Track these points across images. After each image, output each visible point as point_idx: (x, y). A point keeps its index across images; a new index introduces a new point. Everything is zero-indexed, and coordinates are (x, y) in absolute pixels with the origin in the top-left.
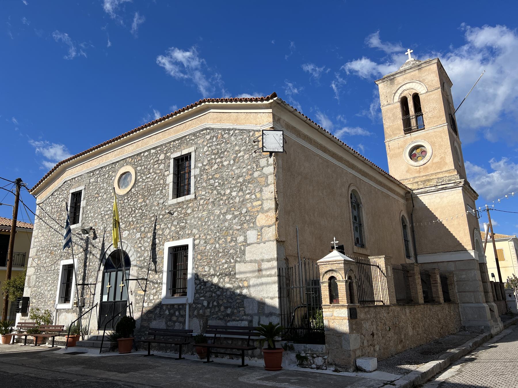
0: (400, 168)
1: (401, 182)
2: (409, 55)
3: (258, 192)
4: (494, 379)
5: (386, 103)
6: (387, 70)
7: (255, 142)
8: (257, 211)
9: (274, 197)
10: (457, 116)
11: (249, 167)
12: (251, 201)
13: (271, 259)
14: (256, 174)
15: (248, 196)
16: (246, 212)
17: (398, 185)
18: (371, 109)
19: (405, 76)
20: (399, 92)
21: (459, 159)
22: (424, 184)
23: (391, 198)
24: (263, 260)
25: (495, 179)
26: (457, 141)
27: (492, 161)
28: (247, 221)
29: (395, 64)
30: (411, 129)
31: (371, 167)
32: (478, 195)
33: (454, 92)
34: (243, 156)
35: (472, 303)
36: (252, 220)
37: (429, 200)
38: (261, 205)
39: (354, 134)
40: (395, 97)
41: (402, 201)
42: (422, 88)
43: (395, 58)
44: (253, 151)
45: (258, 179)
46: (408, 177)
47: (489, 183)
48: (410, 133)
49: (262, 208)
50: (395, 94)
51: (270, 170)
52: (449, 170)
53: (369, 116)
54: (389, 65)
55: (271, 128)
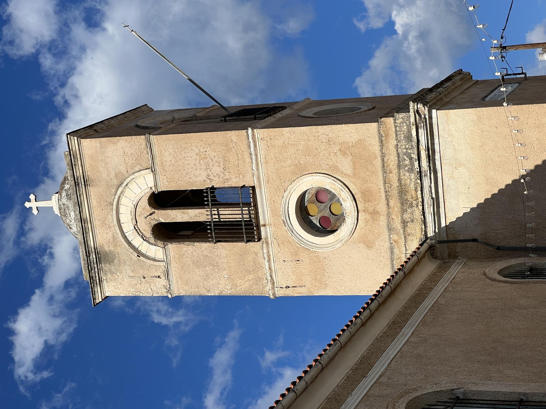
0: (356, 265)
1: (397, 266)
2: (41, 204)
5: (163, 281)
6: (64, 263)
10: (235, 101)
17: (406, 275)
18: (164, 321)
19: (96, 223)
20: (137, 241)
21: (352, 110)
22: (411, 206)
23: (442, 301)
25: (414, 20)
26: (301, 110)
27: (361, 26)
29: (51, 240)
30: (249, 224)
31: (341, 345)
32: (460, 72)
33: (164, 103)
37: (461, 196)
39: (229, 376)
40: (151, 254)
41: (456, 270)
42: (140, 181)
43: (34, 238)
46: (387, 245)
47: (423, 35)
48: (258, 227)
50: (140, 254)
52: (380, 136)
53: (186, 329)
54: (52, 255)
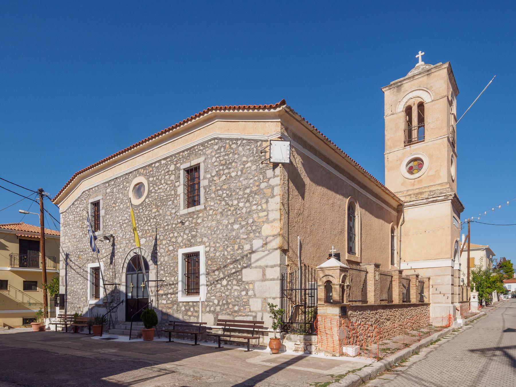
5: (390, 113)
7: (261, 153)
11: (256, 178)
12: (258, 212)
14: (263, 185)
15: (254, 207)
16: (253, 222)
19: (412, 82)
22: (416, 197)
24: (267, 266)
28: (254, 231)
34: (250, 167)
36: (258, 231)
44: (260, 162)
45: (264, 190)
48: (410, 145)
49: (268, 219)
51: (276, 181)
52: (442, 184)
55: (279, 138)
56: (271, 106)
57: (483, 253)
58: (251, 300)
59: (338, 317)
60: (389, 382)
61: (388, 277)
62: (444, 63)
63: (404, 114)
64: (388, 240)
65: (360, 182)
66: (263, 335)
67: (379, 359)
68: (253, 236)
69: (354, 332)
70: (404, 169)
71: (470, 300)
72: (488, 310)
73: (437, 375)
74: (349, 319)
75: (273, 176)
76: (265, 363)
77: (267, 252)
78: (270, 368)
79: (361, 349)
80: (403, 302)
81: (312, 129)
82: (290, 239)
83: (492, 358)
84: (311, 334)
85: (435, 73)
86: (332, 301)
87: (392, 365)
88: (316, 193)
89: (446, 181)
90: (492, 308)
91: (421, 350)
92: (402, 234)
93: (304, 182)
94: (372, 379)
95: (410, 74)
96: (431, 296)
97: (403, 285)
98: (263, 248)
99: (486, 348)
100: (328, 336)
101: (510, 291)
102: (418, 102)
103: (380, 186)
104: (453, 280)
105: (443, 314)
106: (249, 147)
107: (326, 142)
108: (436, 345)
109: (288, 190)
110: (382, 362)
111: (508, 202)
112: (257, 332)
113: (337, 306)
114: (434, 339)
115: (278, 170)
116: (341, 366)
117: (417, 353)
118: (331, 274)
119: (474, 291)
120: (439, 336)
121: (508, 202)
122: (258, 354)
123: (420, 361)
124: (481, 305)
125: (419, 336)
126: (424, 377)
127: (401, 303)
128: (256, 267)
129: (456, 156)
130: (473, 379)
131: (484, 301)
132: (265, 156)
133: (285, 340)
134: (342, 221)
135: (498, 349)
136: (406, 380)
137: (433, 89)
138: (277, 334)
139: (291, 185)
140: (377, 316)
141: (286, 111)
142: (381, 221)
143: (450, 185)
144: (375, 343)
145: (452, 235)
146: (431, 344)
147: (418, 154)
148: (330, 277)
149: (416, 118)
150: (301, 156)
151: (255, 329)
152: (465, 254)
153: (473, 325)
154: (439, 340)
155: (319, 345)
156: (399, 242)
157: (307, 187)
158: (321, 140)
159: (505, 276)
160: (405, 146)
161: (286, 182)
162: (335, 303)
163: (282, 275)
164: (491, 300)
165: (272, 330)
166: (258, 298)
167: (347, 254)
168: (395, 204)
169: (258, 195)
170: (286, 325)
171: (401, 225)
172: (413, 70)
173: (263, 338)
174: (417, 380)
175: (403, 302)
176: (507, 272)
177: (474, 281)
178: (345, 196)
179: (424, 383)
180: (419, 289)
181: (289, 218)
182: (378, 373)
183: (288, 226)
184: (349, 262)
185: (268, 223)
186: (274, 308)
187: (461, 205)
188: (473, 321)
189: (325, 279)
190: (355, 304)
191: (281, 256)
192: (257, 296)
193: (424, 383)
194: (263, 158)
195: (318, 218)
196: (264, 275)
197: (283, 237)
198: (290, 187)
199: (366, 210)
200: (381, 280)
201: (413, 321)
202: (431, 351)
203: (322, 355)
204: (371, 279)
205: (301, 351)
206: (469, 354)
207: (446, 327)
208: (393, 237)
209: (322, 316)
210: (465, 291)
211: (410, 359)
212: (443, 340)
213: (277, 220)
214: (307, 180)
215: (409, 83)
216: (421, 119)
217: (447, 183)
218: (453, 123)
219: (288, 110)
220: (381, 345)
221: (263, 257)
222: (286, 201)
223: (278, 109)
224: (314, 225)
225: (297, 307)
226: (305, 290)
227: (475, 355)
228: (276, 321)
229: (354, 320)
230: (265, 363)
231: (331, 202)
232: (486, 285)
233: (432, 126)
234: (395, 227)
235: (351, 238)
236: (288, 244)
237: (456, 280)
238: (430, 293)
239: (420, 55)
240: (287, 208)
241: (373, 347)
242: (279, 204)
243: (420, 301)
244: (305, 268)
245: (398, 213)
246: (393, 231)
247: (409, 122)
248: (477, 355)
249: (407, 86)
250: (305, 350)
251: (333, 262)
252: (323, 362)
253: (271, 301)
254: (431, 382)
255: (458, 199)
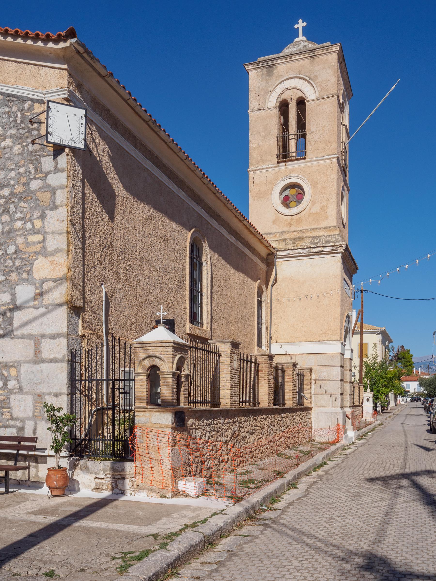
3: (38, 218)
4: (347, 502)
5: (257, 107)
7: (32, 123)
8: (36, 252)
9: (65, 229)
11: (22, 170)
12: (25, 233)
13: (58, 334)
14: (35, 185)
15: (19, 224)
16: (16, 252)
17: (260, 240)
19: (289, 65)
20: (279, 90)
22: (293, 243)
24: (43, 336)
28: (18, 268)
34: (11, 148)
35: (329, 407)
36: (25, 268)
38: (43, 241)
44: (29, 141)
45: (38, 194)
46: (274, 231)
48: (285, 161)
49: (44, 248)
51: (59, 179)
52: (329, 227)
55: (65, 99)
56: (48, 36)
57: (377, 339)
58: (12, 397)
59: (170, 430)
60: (252, 541)
61: (252, 365)
62: (333, 43)
63: (276, 112)
64: (253, 307)
65: (210, 208)
66: (37, 462)
67: (237, 500)
68: (16, 279)
69: (197, 454)
70: (276, 198)
71: (362, 403)
72: (385, 417)
73: (325, 524)
74: (189, 433)
75: (53, 169)
76: (33, 518)
77: (42, 310)
78: (41, 527)
79: (207, 483)
80: (275, 404)
81: (127, 97)
82: (87, 289)
83: (397, 491)
84: (124, 459)
85: (322, 57)
86: (159, 401)
87: (257, 508)
88: (137, 217)
89: (335, 224)
90: (389, 415)
91: (299, 481)
92: (273, 299)
93: (113, 191)
94: (224, 537)
95: (286, 51)
96: (313, 396)
97: (274, 379)
98: (36, 302)
99: (387, 475)
100: (153, 462)
101: (409, 392)
102: (297, 97)
103: (242, 219)
104: (342, 374)
105: (330, 424)
106: (7, 109)
107: (153, 125)
108: (320, 472)
109: (83, 198)
110: (242, 506)
111: (417, 261)
112: (26, 458)
113: (168, 411)
114: (318, 463)
115: (63, 160)
116: (174, 515)
117: (294, 486)
118: (157, 354)
119: (368, 390)
120: (324, 458)
121: (417, 261)
122: (24, 498)
123: (299, 499)
124: (376, 410)
125: (297, 457)
126: (306, 529)
127: (272, 406)
128: (23, 337)
129: (348, 190)
130: (376, 529)
131: (380, 406)
132: (38, 129)
133: (77, 471)
134: (181, 267)
135: (404, 476)
136: (278, 535)
137: (318, 80)
138: (61, 460)
139: (89, 190)
140: (235, 428)
141: (78, 52)
142: (242, 275)
143: (340, 231)
144: (232, 471)
145: (342, 306)
146: (314, 471)
147: (297, 178)
148: (156, 359)
149: (294, 116)
150: (107, 143)
151: (21, 452)
152: (357, 338)
153: (367, 440)
154: (325, 463)
155: (138, 478)
156: (269, 312)
157: (119, 200)
158: (144, 120)
159: (404, 371)
160: (278, 163)
161: (79, 184)
162: (164, 406)
163: (72, 353)
164: (388, 403)
165: (52, 453)
166: (26, 393)
167: (188, 324)
168: (263, 252)
169: (26, 202)
170: (80, 444)
171: (272, 286)
172: (290, 46)
173: (37, 467)
174: (295, 535)
175: (275, 404)
176: (406, 366)
177: (367, 377)
178: (187, 226)
179: (305, 539)
180: (297, 385)
181: (84, 251)
182: (236, 524)
183: (84, 265)
184: (192, 337)
185: (45, 256)
186: (56, 413)
187: (355, 263)
188: (367, 433)
189: (148, 363)
190: (200, 407)
191: (70, 318)
192: (25, 390)
193: (305, 539)
194: (35, 133)
195: (139, 257)
196: (38, 351)
197: (74, 284)
198: (87, 195)
199: (220, 255)
200: (242, 369)
201: (288, 435)
202: (315, 482)
203: (142, 497)
204: (226, 366)
205: (106, 490)
206: (367, 485)
207: (334, 443)
208: (260, 303)
209: (142, 428)
210: (356, 390)
211: (284, 496)
212: (330, 464)
213: (61, 251)
214: (119, 188)
215: (285, 65)
216: (301, 125)
217: (336, 227)
218: (344, 139)
219: (81, 50)
220: (241, 474)
221: (35, 319)
222: (78, 218)
223: (62, 45)
224: (132, 268)
225: (101, 411)
226: (114, 381)
227: (376, 487)
228: (59, 437)
229: (197, 434)
230: (33, 518)
231: (161, 232)
232: (382, 381)
233: (316, 137)
234: (264, 287)
235: (195, 298)
236: (84, 298)
237: (347, 373)
238: (312, 393)
239: (301, 25)
240: (80, 231)
241: (228, 479)
242: (65, 222)
243: (298, 404)
244: (114, 341)
245: (267, 266)
246: (260, 294)
247: (285, 126)
248: (378, 486)
249: (282, 68)
250: (113, 489)
251: (161, 334)
252: (142, 509)
253: (50, 400)
254: (317, 538)
255: (350, 253)
